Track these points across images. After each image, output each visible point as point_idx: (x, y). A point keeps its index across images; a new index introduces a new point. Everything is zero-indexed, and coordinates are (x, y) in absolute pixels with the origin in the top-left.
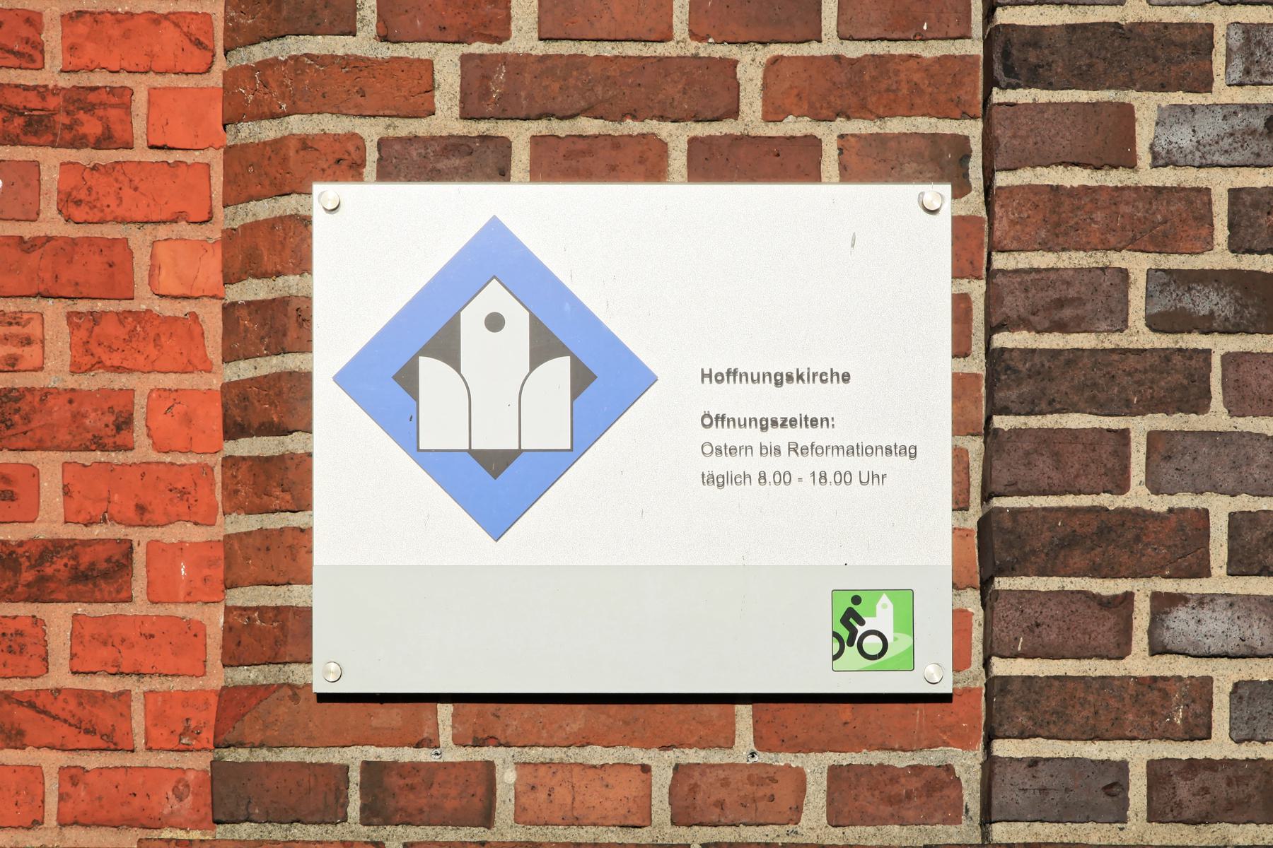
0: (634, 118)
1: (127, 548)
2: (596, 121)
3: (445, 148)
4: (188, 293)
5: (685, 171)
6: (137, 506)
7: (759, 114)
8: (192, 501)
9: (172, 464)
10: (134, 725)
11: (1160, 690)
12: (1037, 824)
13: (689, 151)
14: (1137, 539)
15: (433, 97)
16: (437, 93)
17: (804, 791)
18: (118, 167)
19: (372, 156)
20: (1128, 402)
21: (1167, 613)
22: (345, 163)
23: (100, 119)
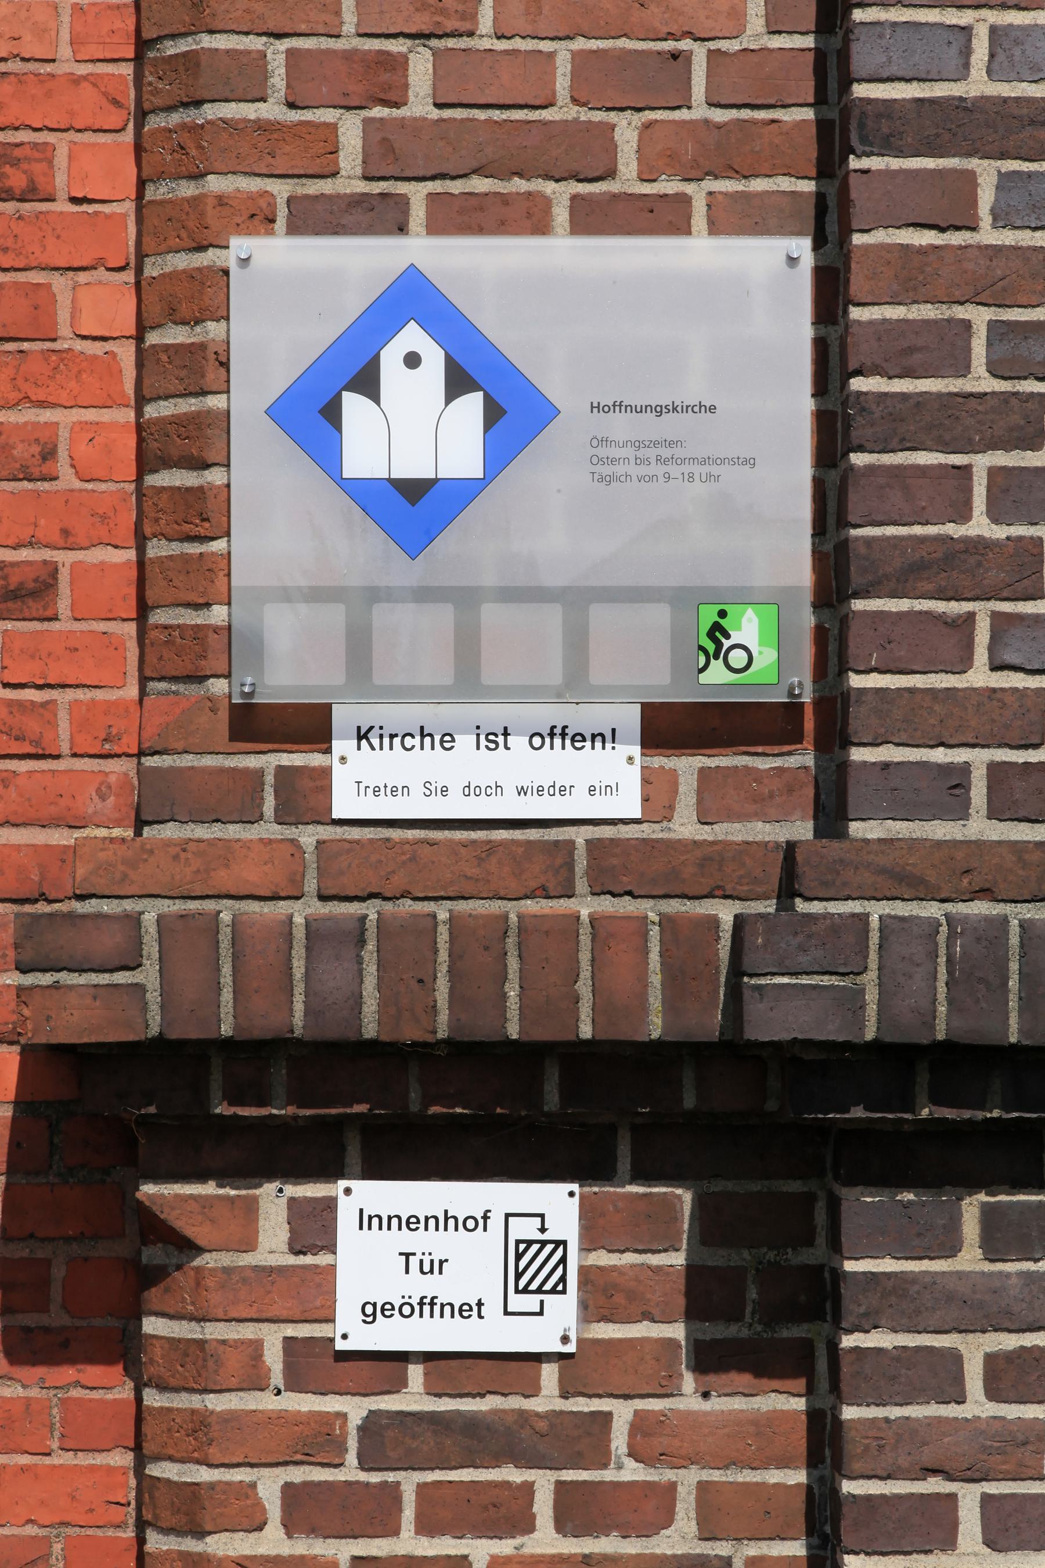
0: (520, 175)
1: (53, 570)
2: (486, 180)
3: (349, 205)
4: (107, 334)
5: (567, 225)
6: (61, 530)
7: (635, 174)
8: (112, 525)
9: (94, 491)
10: (60, 732)
11: (999, 701)
12: (890, 822)
13: (571, 207)
14: (979, 564)
15: (337, 158)
16: (341, 153)
17: (676, 792)
18: (42, 217)
19: (282, 213)
20: (970, 440)
21: (1005, 631)
22: (260, 218)
23: (25, 172)
